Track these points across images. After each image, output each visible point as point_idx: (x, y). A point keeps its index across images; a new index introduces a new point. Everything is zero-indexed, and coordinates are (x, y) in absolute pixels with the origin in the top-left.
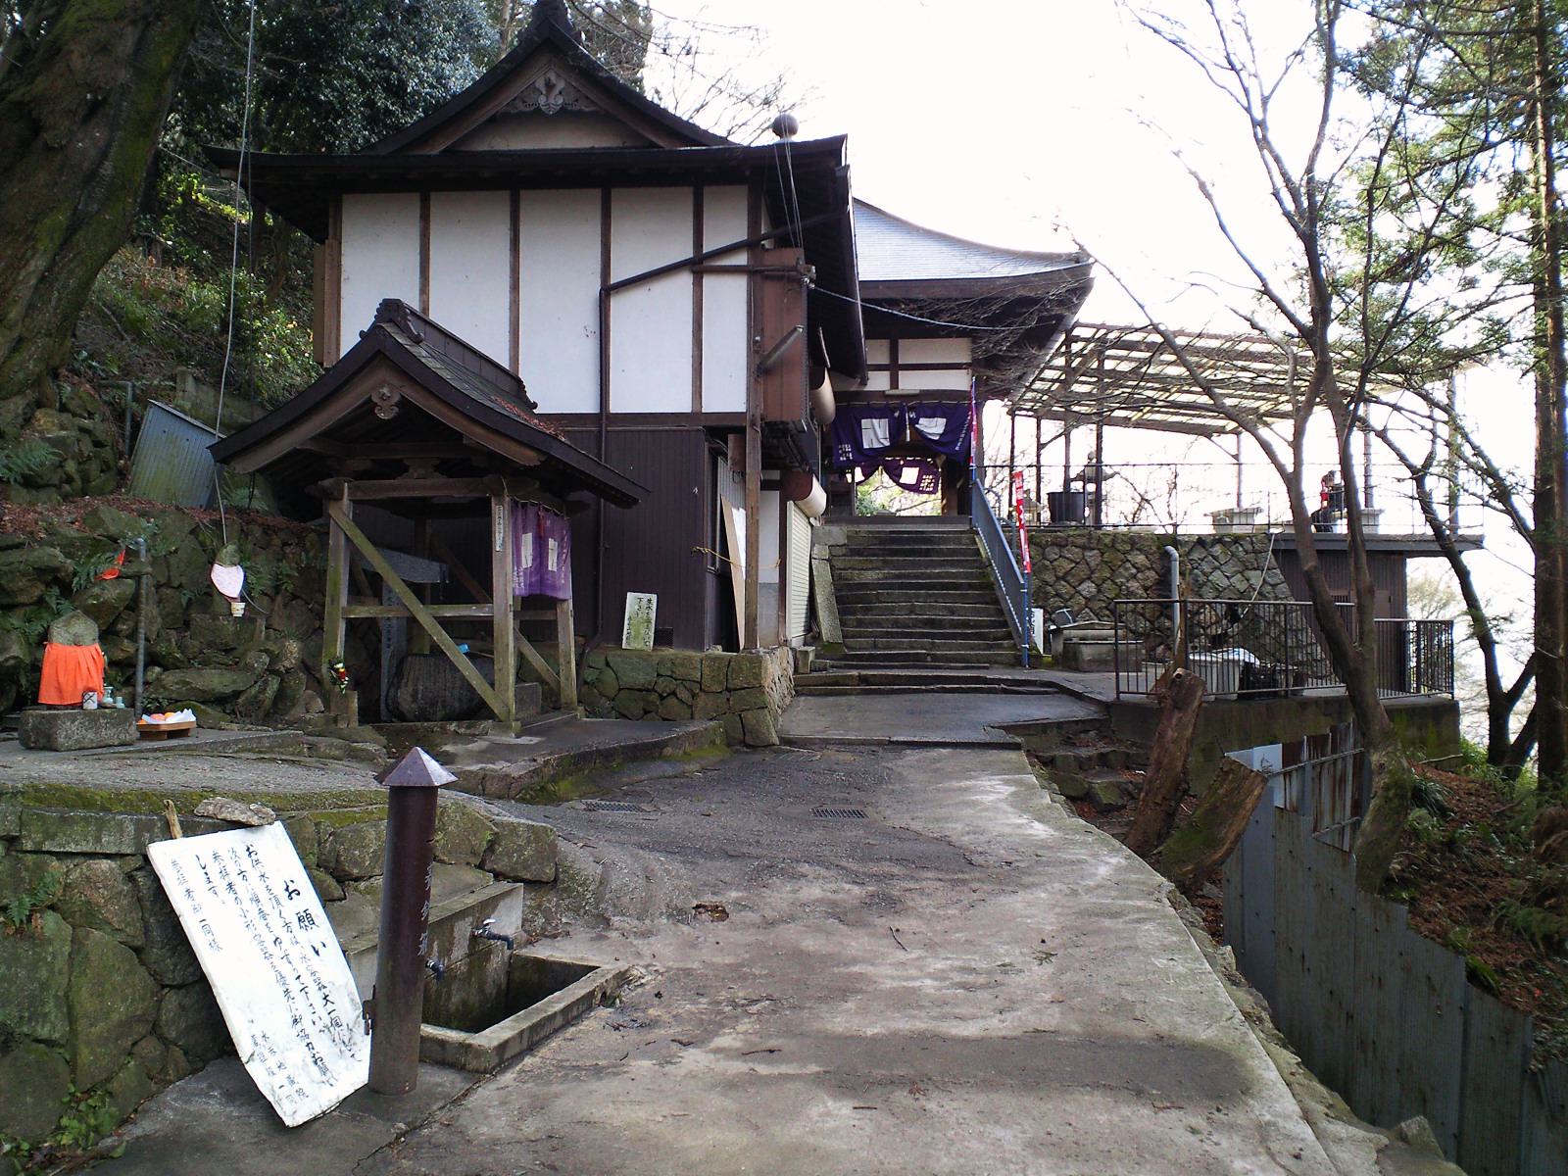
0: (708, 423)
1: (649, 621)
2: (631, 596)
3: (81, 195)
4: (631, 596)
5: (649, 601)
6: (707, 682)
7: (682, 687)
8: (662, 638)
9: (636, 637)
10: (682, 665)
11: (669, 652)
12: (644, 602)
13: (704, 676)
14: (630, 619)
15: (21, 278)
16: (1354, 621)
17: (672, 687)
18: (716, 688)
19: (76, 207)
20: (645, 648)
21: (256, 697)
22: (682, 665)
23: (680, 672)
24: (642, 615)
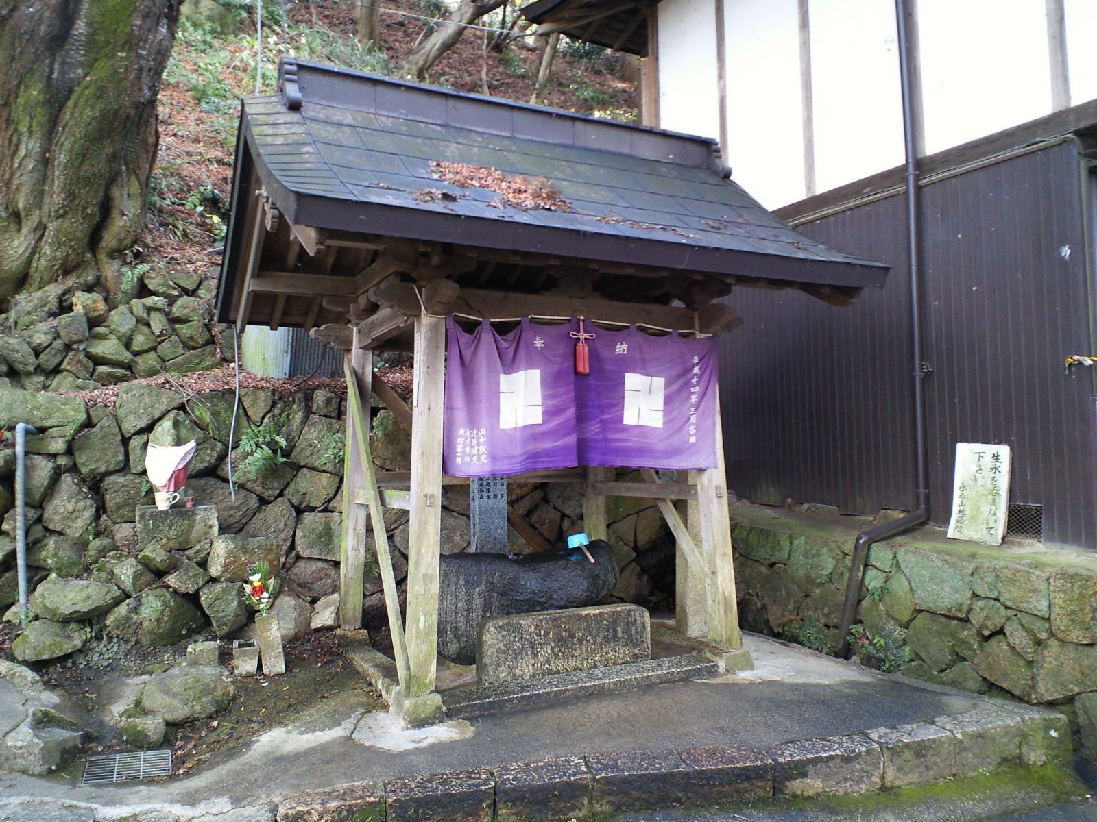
0: (1083, 124)
1: (995, 492)
2: (964, 451)
3: (52, 63)
4: (964, 451)
5: (996, 457)
6: (1060, 622)
7: (1015, 625)
8: (1022, 521)
9: (973, 519)
10: (1012, 581)
11: (1033, 549)
12: (987, 461)
13: (1056, 609)
14: (963, 487)
15: (16, 165)
16: (968, 399)
17: (998, 621)
18: (1076, 635)
19: (49, 78)
20: (988, 539)
21: (127, 618)
22: (1012, 581)
23: (1010, 594)
24: (986, 479)
